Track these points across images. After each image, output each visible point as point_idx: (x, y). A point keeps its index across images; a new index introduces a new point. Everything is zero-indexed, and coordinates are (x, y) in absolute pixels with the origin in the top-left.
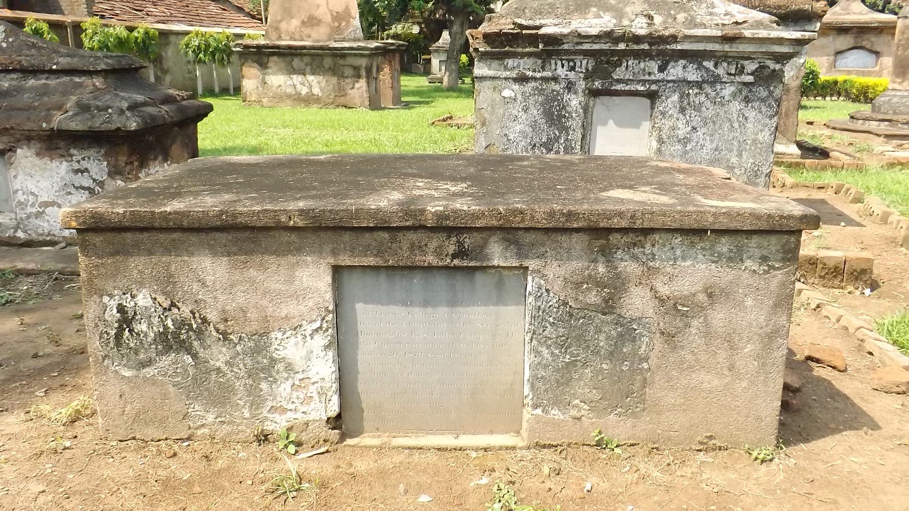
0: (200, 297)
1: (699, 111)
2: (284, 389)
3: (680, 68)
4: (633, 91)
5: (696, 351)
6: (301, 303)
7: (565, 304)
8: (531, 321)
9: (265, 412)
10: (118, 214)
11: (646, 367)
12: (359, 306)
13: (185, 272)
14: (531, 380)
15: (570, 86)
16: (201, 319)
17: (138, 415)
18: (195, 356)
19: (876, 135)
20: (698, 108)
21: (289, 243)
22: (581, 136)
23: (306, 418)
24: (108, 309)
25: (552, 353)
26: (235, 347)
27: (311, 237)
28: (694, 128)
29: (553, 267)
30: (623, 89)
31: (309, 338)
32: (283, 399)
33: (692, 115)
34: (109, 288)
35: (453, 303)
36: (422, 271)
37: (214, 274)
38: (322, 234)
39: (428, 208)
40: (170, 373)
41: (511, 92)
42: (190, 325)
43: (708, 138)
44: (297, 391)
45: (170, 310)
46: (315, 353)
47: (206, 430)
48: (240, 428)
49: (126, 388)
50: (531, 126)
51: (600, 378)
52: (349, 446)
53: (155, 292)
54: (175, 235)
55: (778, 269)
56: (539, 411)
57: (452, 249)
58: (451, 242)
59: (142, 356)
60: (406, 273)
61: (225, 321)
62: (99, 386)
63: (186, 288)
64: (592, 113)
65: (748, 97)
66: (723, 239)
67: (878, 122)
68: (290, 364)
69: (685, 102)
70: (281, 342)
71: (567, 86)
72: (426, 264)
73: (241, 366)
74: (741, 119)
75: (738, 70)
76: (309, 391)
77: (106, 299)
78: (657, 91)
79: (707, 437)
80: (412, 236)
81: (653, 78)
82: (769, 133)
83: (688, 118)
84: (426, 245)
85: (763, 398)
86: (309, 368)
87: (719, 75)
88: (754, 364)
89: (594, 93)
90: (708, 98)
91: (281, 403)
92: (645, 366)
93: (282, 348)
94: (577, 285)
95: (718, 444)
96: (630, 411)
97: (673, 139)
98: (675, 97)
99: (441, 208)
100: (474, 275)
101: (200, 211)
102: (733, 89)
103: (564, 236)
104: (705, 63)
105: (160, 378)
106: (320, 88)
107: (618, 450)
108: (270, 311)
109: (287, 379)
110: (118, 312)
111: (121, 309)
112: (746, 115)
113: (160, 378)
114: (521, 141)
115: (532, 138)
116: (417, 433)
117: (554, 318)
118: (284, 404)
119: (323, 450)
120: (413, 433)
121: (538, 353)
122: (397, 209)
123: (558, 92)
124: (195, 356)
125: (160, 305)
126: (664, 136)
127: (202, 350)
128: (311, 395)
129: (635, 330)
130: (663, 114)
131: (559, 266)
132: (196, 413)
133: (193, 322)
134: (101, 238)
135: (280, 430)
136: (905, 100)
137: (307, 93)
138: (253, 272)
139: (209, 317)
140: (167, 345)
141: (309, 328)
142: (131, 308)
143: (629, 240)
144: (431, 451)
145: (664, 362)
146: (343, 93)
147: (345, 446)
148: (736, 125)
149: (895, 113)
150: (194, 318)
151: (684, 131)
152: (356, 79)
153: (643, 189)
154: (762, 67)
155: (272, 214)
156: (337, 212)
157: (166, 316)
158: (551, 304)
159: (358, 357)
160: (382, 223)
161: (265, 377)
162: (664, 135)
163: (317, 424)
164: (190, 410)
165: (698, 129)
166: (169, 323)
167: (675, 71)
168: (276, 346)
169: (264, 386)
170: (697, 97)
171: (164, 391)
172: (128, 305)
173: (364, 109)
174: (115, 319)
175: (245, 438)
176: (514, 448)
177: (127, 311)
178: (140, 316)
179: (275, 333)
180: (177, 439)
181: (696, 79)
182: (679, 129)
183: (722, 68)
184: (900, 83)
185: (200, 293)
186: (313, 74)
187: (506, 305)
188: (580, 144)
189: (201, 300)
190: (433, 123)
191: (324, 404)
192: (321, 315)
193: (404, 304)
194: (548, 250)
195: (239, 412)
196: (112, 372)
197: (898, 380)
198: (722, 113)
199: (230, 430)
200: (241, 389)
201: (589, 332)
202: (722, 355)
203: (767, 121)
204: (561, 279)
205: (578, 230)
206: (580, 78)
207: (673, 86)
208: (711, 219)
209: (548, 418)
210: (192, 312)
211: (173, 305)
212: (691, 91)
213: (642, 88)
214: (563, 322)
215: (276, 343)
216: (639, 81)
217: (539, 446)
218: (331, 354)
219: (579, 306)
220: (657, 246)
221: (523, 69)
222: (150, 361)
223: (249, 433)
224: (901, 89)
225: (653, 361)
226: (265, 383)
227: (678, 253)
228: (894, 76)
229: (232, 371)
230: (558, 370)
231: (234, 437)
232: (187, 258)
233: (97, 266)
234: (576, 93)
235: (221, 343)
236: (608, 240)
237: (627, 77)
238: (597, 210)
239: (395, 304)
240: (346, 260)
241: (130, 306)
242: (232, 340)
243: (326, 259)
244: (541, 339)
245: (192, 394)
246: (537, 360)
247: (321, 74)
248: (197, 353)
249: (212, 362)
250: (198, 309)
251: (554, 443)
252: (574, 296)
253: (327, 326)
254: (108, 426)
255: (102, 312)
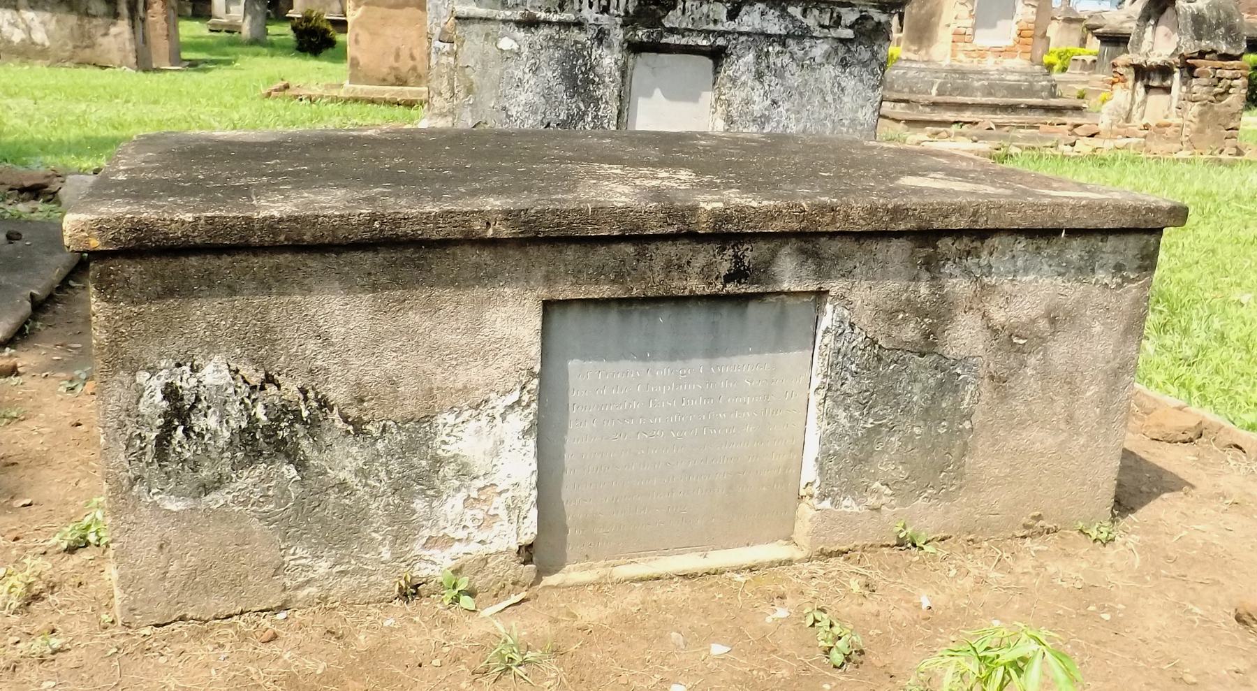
0: (319, 363)
1: (782, 77)
2: (452, 506)
3: (757, 15)
4: (691, 45)
5: (1030, 399)
6: (490, 363)
7: (874, 343)
8: (827, 372)
9: (417, 548)
10: (183, 222)
11: (967, 427)
12: (573, 365)
13: (294, 321)
14: (820, 459)
15: (601, 36)
16: (318, 401)
17: (192, 575)
18: (301, 466)
19: (893, 119)
20: (780, 73)
21: (477, 266)
22: (617, 112)
23: (484, 550)
24: (147, 392)
25: (851, 417)
26: (373, 444)
27: (514, 254)
28: (774, 102)
29: (862, 289)
30: (677, 42)
31: (499, 419)
32: (450, 523)
33: (772, 84)
34: (151, 358)
35: (713, 352)
36: (673, 304)
37: (347, 322)
38: (533, 251)
39: (702, 205)
40: (255, 498)
41: (512, 42)
42: (297, 413)
43: (793, 116)
44: (473, 508)
45: (263, 388)
46: (507, 444)
47: (312, 590)
48: (373, 578)
49: (172, 533)
50: (543, 95)
51: (910, 447)
52: (552, 587)
53: (237, 359)
54: (282, 259)
55: (1132, 281)
56: (827, 504)
57: (725, 267)
58: (725, 257)
59: (205, 473)
60: (647, 308)
61: (358, 402)
62: (121, 533)
63: (294, 350)
64: (631, 77)
65: (845, 58)
66: (1075, 242)
67: (893, 103)
68: (464, 465)
69: (763, 64)
70: (452, 431)
71: (598, 35)
72: (687, 293)
73: (383, 475)
74: (836, 90)
75: (832, 21)
76: (493, 506)
77: (142, 377)
78: (726, 47)
79: (1034, 517)
80: (669, 249)
81: (719, 27)
82: (872, 110)
83: (767, 87)
84: (689, 263)
85: (1102, 458)
86: (495, 469)
87: (808, 27)
88: (1095, 412)
89: (635, 48)
90: (793, 59)
91: (445, 531)
92: (967, 425)
93: (452, 439)
94: (891, 315)
95: (1048, 526)
96: (944, 490)
97: (746, 117)
98: (750, 57)
99: (720, 205)
100: (747, 306)
101: (336, 216)
102: (826, 47)
103: (880, 243)
104: (791, 10)
105: (236, 509)
106: (47, 32)
107: (928, 548)
108: (437, 380)
109: (458, 490)
110: (164, 398)
111: (171, 393)
112: (843, 84)
113: (236, 509)
114: (528, 118)
115: (544, 113)
116: (645, 556)
117: (857, 365)
118: (450, 531)
119: (515, 599)
120: (640, 557)
121: (831, 418)
122: (656, 207)
123: (584, 45)
124: (301, 466)
125: (245, 382)
126: (734, 113)
127: (316, 453)
128: (496, 512)
129: (959, 375)
130: (733, 80)
131: (871, 288)
132: (298, 562)
133: (303, 407)
134: (140, 268)
135: (440, 574)
136: (922, 74)
137: (23, 40)
138: (413, 317)
139: (332, 396)
140: (252, 451)
141: (500, 404)
142: (189, 390)
143: (962, 247)
144: (675, 580)
145: (990, 419)
146: (87, 42)
147: (545, 587)
148: (830, 98)
149: (911, 91)
150: (306, 399)
151: (760, 106)
152: (111, 20)
153: (932, 175)
154: (864, 18)
155: (458, 218)
156: (565, 214)
157: (254, 400)
158: (854, 344)
159: (567, 447)
160: (631, 230)
161: (422, 489)
162: (734, 112)
163: (502, 558)
164: (287, 559)
165: (780, 103)
166: (260, 412)
167: (750, 19)
168: (445, 438)
169: (419, 504)
170: (779, 57)
171: (242, 531)
172: (184, 384)
173: (128, 70)
174: (159, 411)
175: (380, 595)
176: (789, 562)
177: (183, 395)
178: (205, 404)
179: (445, 415)
180: (262, 611)
181: (779, 32)
182: (754, 103)
183: (812, 17)
184: (916, 52)
185: (319, 357)
186: (32, 8)
187: (786, 350)
188: (615, 123)
189: (320, 369)
190: (269, 94)
191: (515, 524)
192: (521, 381)
193: (643, 358)
194: (858, 265)
195: (373, 553)
196: (147, 507)
197: (1183, 425)
198: (812, 81)
199: (355, 585)
200: (380, 513)
201: (901, 382)
202: (1061, 402)
203: (870, 93)
204: (871, 307)
205: (899, 234)
206: (617, 24)
207: (747, 41)
208: (1068, 215)
209: (838, 512)
210: (303, 391)
211: (269, 379)
212: (771, 49)
213: (705, 43)
214: (869, 370)
215: (445, 433)
216: (700, 32)
217: (824, 554)
218: (531, 443)
219: (890, 346)
220: (995, 254)
221: (531, 7)
222: (220, 481)
223: (390, 585)
224: (917, 59)
225: (978, 418)
226: (420, 499)
227: (1020, 263)
228: (908, 42)
229: (366, 485)
230: (856, 442)
231: (361, 595)
232: (299, 298)
233: (128, 318)
234: (609, 47)
235: (350, 439)
236: (936, 247)
237: (684, 25)
238: (932, 204)
239: (626, 358)
240: (566, 291)
241: (189, 387)
242: (369, 433)
243: (535, 290)
244: (838, 397)
245: (293, 530)
246: (830, 428)
247: (48, 8)
248: (306, 460)
249: (331, 473)
250: (314, 384)
251: (844, 548)
252: (886, 331)
253: (530, 398)
254: (134, 601)
255: (134, 401)
